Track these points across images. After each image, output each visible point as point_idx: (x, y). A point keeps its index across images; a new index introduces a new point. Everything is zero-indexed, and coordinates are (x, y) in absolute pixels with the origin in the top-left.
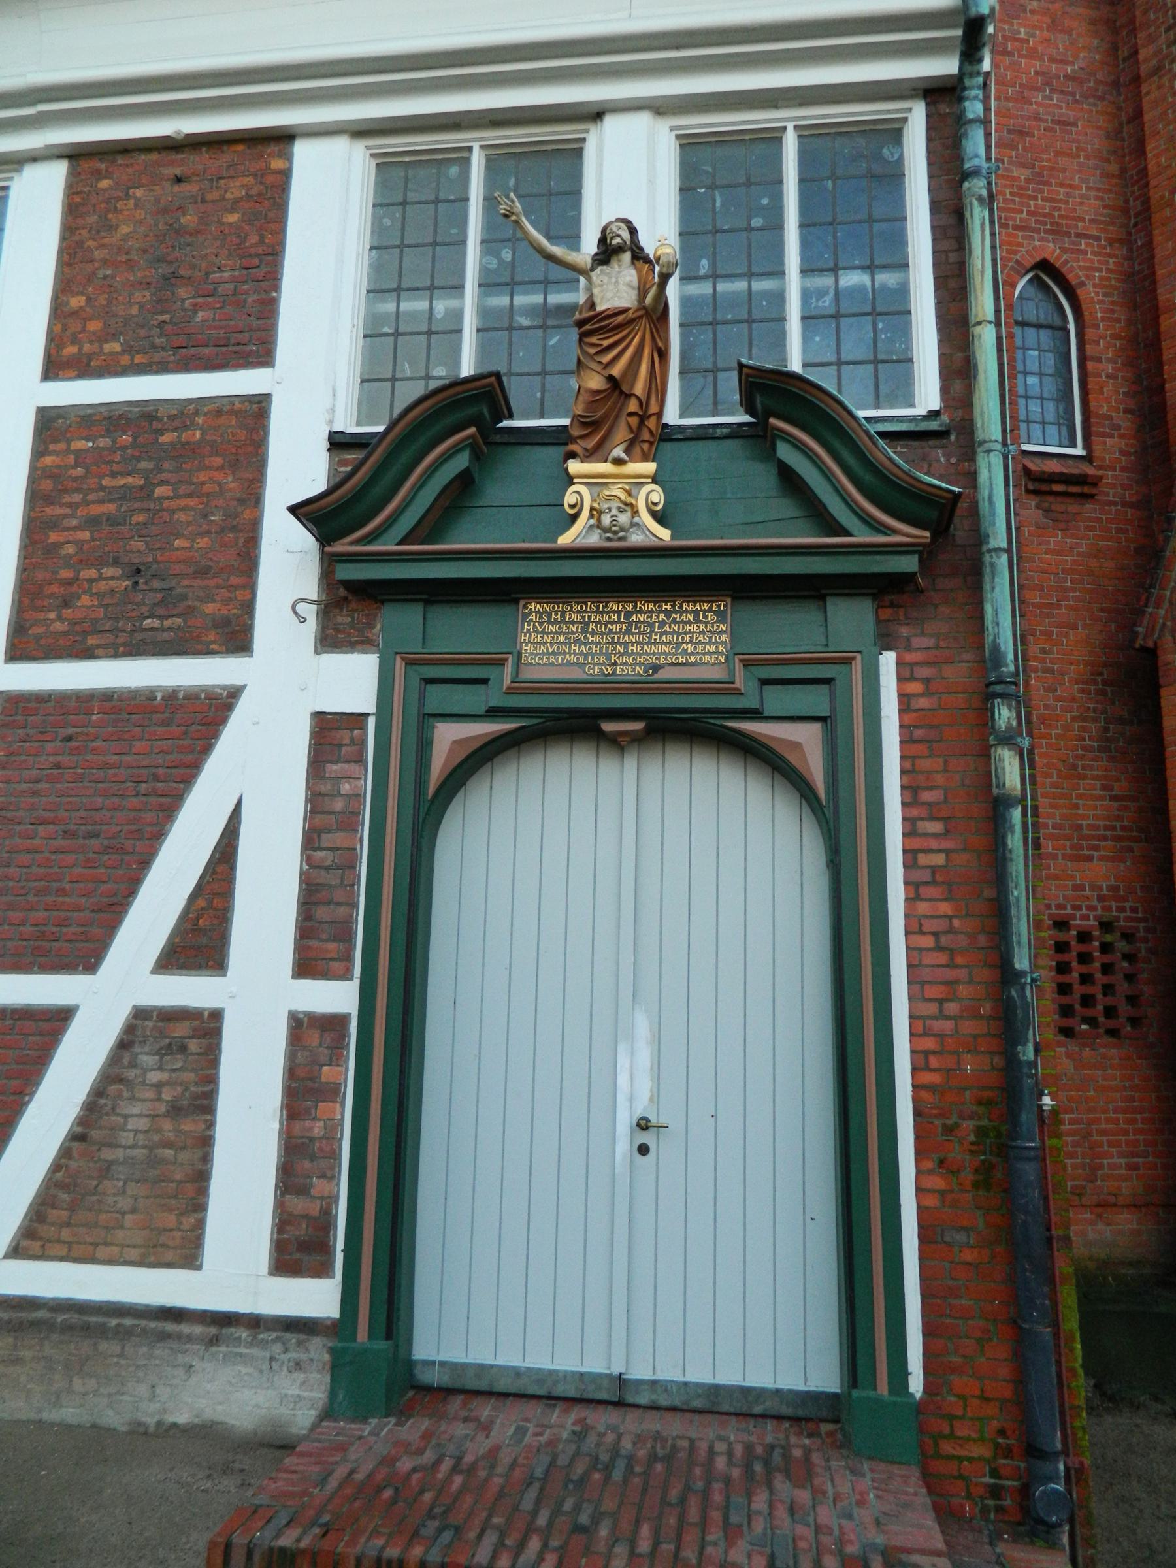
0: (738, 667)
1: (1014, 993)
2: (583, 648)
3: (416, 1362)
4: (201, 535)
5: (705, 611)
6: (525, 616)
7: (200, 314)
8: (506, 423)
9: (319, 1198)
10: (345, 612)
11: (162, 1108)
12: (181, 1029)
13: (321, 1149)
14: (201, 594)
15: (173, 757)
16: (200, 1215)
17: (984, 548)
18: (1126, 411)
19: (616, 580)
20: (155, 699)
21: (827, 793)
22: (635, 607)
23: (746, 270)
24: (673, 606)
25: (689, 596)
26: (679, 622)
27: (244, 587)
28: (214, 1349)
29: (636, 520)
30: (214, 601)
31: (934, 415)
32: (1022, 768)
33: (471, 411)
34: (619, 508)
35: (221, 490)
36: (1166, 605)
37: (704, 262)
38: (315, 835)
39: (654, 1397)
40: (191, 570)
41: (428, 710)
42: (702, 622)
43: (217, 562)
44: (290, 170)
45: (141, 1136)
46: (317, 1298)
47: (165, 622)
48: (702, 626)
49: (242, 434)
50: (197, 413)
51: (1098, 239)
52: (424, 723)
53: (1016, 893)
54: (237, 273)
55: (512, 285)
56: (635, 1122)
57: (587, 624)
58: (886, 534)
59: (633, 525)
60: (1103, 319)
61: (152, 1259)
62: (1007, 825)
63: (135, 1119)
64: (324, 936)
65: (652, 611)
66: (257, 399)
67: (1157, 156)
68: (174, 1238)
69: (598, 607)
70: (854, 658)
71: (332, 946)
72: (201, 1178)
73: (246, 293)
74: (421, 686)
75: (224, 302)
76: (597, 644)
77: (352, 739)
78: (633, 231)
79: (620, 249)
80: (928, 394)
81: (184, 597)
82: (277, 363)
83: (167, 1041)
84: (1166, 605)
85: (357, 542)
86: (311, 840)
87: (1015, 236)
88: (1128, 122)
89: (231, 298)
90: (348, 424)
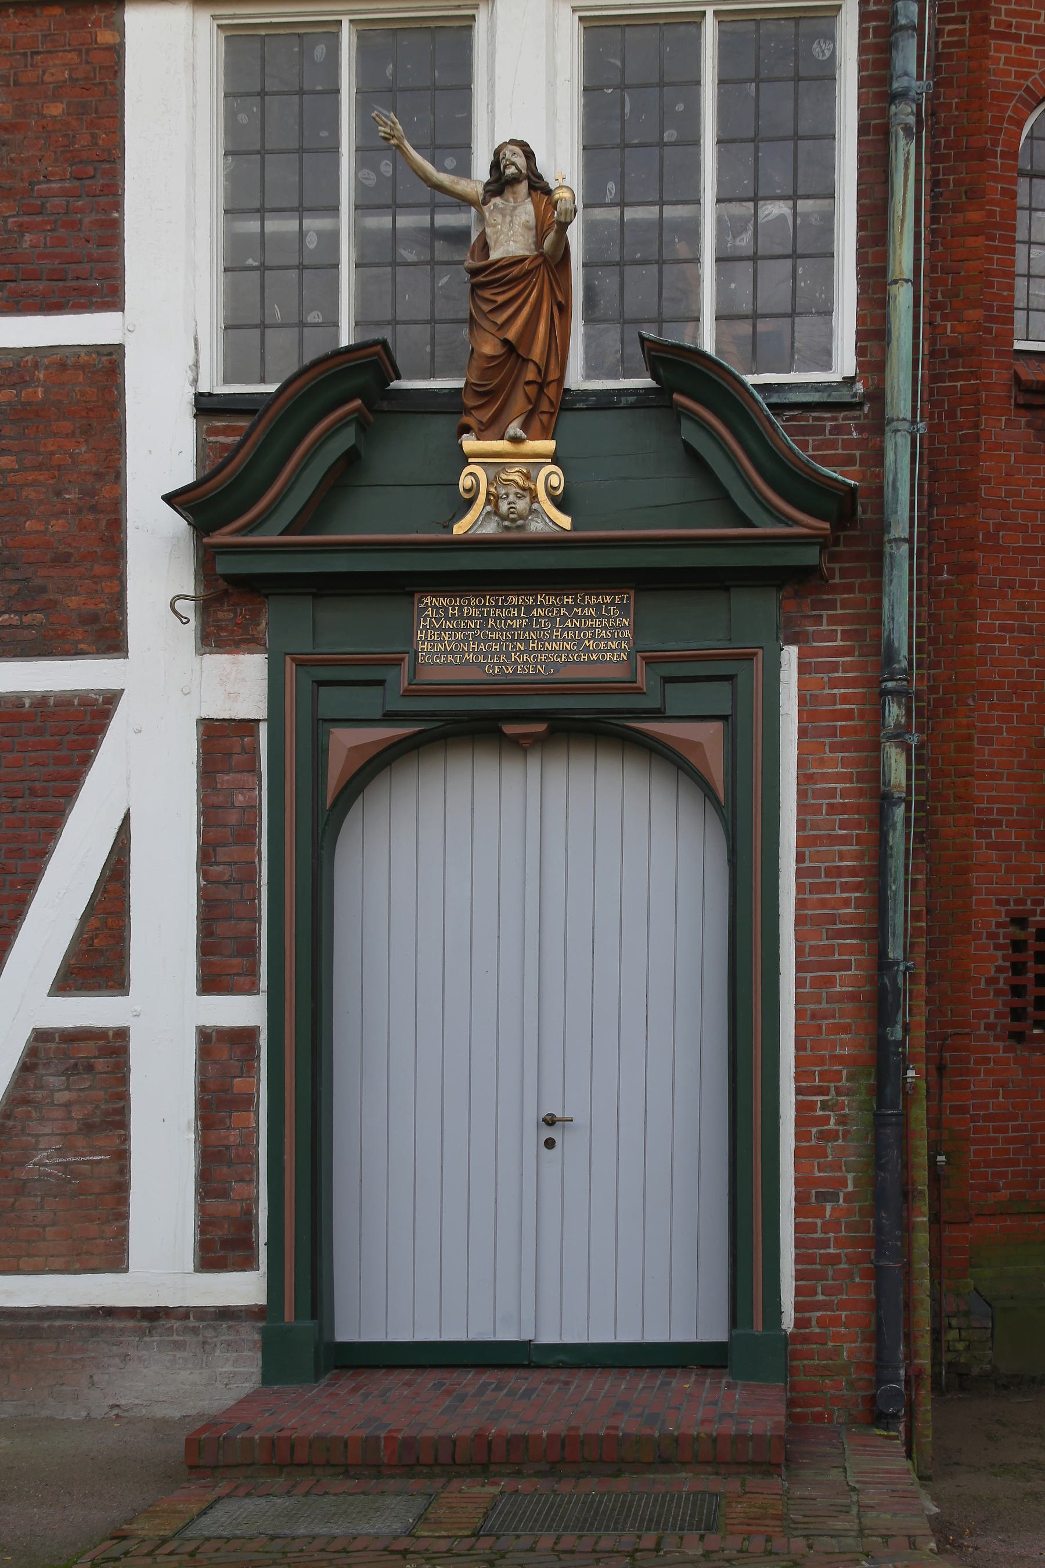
0: (640, 664)
1: (886, 981)
2: (482, 646)
7: (27, 237)
8: (395, 384)
11: (74, 1127)
16: (122, 1223)
19: (513, 570)
20: (23, 705)
22: (536, 600)
23: (657, 198)
24: (575, 600)
25: (587, 589)
26: (581, 617)
28: (147, 1339)
29: (535, 506)
30: (78, 594)
31: (849, 381)
32: (909, 762)
34: (516, 494)
37: (611, 185)
38: (211, 849)
42: (604, 616)
44: (122, 45)
46: (244, 1288)
47: (24, 619)
48: (605, 621)
50: (36, 365)
52: (317, 730)
53: (894, 888)
55: (394, 207)
57: (486, 620)
58: (788, 525)
59: (531, 511)
61: (77, 1266)
63: (47, 1138)
70: (755, 654)
71: (235, 961)
72: (120, 1189)
74: (309, 690)
76: (497, 641)
77: (244, 749)
78: (529, 155)
79: (515, 180)
80: (845, 362)
81: (43, 590)
85: (237, 532)
86: (206, 855)
87: (1029, 52)
90: (211, 383)
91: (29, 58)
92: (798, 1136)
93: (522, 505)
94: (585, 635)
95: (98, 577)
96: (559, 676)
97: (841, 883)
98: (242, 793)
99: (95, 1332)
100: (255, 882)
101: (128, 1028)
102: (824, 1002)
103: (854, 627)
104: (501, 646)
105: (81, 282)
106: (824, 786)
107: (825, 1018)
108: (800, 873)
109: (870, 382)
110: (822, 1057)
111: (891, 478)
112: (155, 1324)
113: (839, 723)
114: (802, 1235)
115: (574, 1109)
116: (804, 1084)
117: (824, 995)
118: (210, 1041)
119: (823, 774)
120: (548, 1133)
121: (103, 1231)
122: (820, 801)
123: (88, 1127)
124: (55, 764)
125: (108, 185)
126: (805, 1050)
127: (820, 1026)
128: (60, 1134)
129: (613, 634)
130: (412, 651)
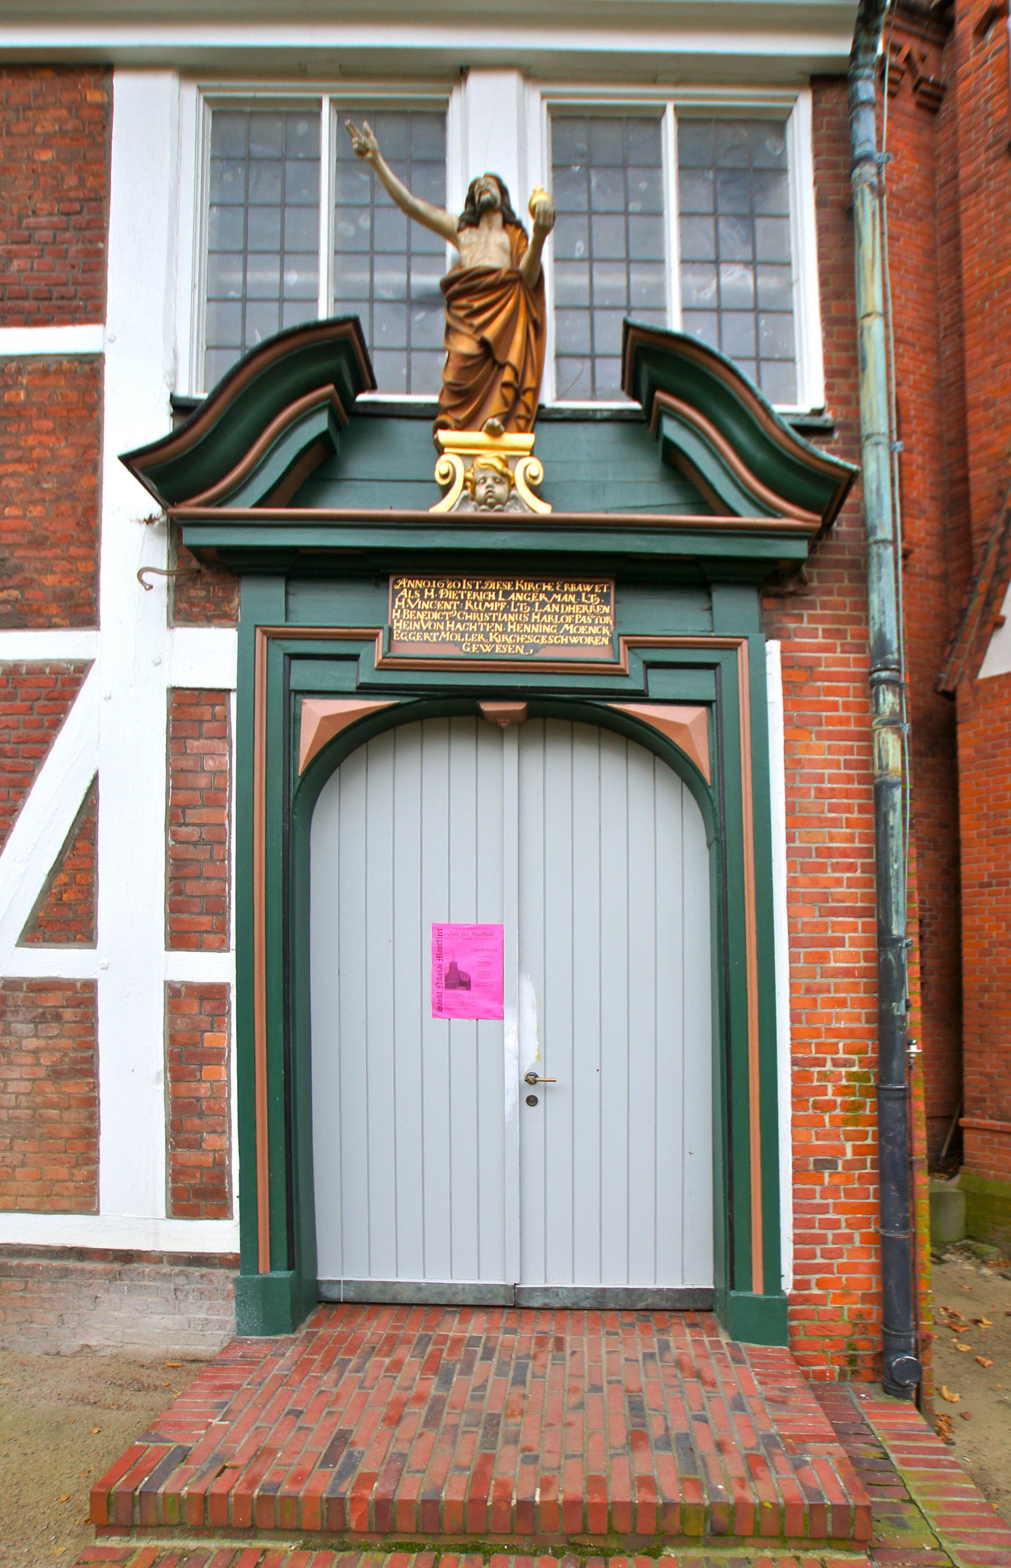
1: (891, 956)
2: (459, 625)
3: (322, 1282)
4: (35, 503)
5: (587, 593)
6: (396, 593)
7: (15, 263)
9: (211, 1151)
10: (198, 585)
11: (42, 1073)
12: (53, 999)
13: (209, 1108)
14: (39, 565)
15: (21, 731)
16: (93, 1168)
17: (871, 540)
18: (932, 498)
21: (712, 773)
22: (514, 586)
24: (554, 587)
26: (560, 603)
27: (85, 558)
28: (118, 1282)
29: (513, 492)
30: (53, 573)
31: (818, 413)
33: (327, 365)
35: (52, 456)
36: (966, 656)
38: (180, 811)
39: (547, 1301)
40: (24, 541)
41: (294, 685)
43: (55, 532)
45: (22, 1098)
46: (222, 1236)
48: (585, 608)
49: (73, 397)
50: (19, 371)
51: (913, 345)
53: (895, 866)
54: (55, 219)
56: (523, 1078)
57: (463, 602)
58: (774, 516)
59: (509, 499)
60: (915, 417)
61: (48, 1206)
62: (890, 803)
63: (15, 1082)
64: (196, 910)
65: (531, 591)
66: (88, 359)
67: (971, 268)
68: (67, 1188)
69: (474, 585)
70: (740, 644)
71: (205, 919)
72: (90, 1135)
73: (69, 242)
74: (283, 657)
75: (42, 250)
76: (474, 622)
77: (214, 716)
78: (504, 191)
82: (108, 320)
83: (40, 1010)
84: (966, 656)
86: (176, 816)
88: (943, 243)
89: (52, 247)
91: (21, 114)
92: (795, 1106)
93: (500, 490)
94: (564, 619)
95: (74, 558)
96: (540, 655)
97: (832, 864)
98: (212, 759)
99: (66, 1273)
100: (224, 843)
101: (96, 981)
102: (819, 976)
103: (834, 626)
104: (478, 627)
105: (65, 303)
106: (812, 771)
107: (820, 991)
108: (790, 852)
109: (839, 414)
110: (818, 1030)
111: (874, 486)
112: (127, 1267)
113: (824, 714)
114: (800, 1201)
115: (554, 1071)
116: (800, 1055)
117: (818, 970)
118: (177, 995)
119: (810, 760)
120: (531, 1091)
121: (73, 1175)
122: (808, 785)
123: (56, 1074)
124: (25, 728)
125: (93, 220)
126: (800, 1022)
127: (815, 1000)
128: (29, 1080)
129: (593, 620)
130: (386, 626)
